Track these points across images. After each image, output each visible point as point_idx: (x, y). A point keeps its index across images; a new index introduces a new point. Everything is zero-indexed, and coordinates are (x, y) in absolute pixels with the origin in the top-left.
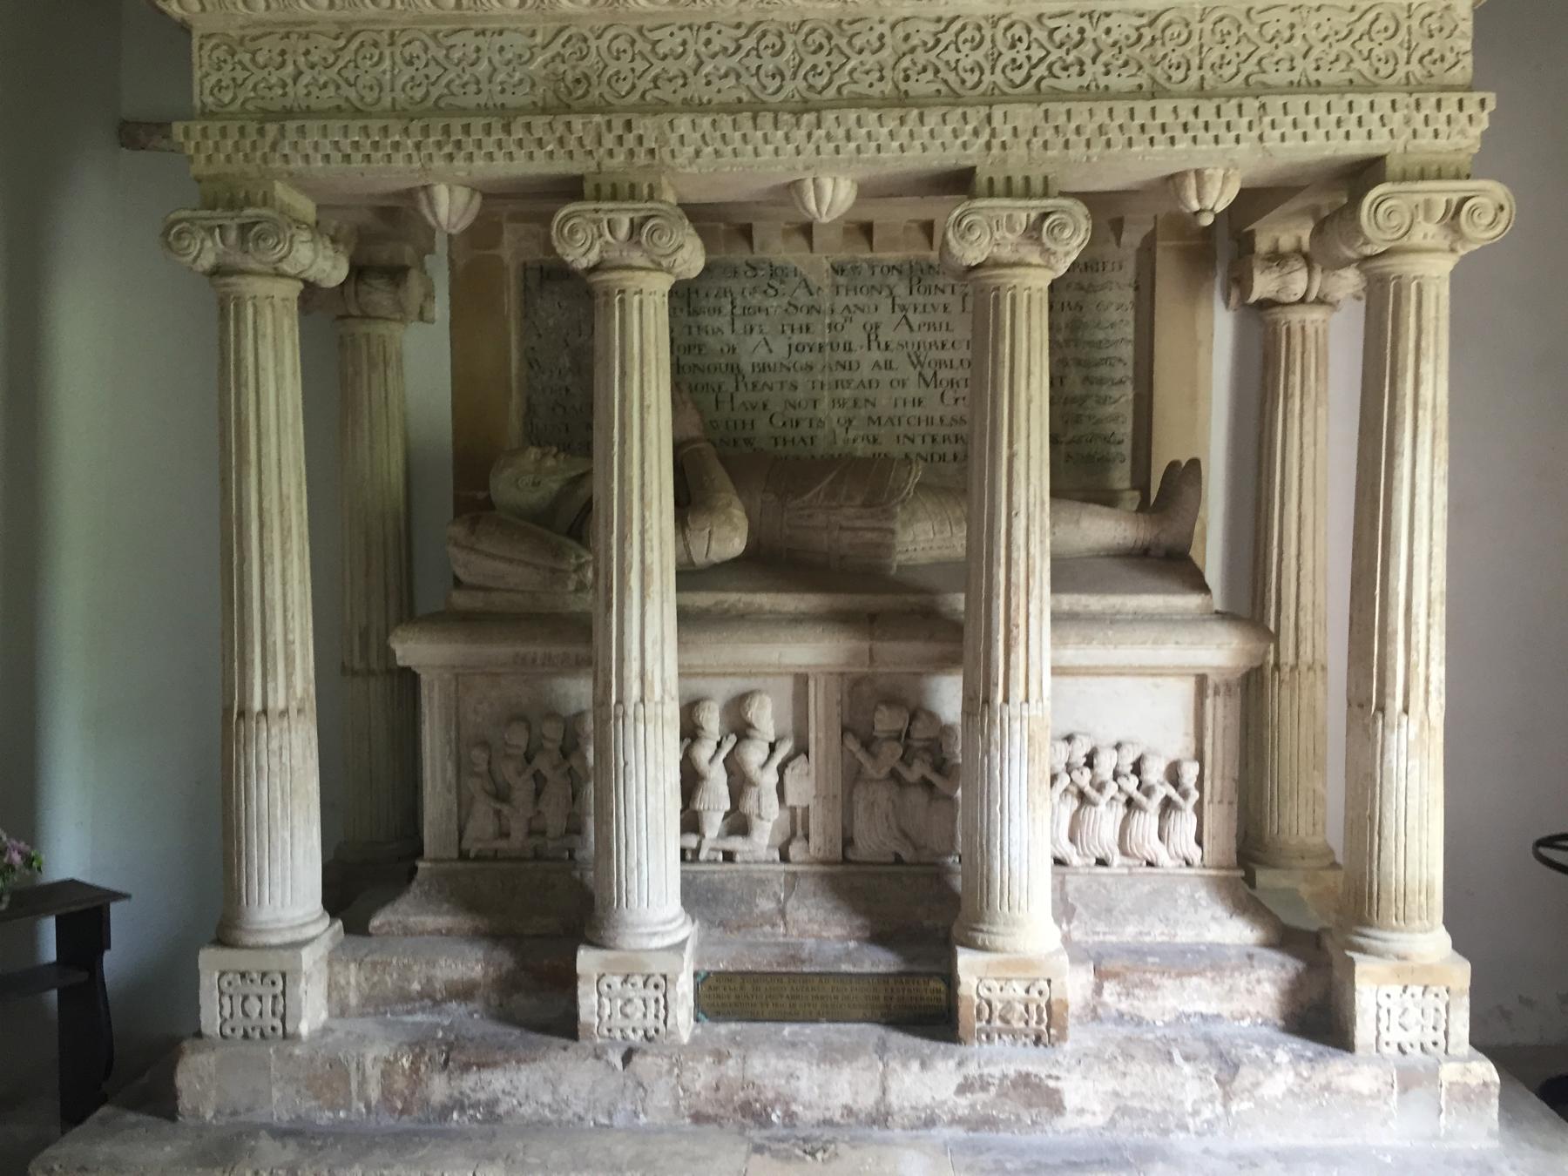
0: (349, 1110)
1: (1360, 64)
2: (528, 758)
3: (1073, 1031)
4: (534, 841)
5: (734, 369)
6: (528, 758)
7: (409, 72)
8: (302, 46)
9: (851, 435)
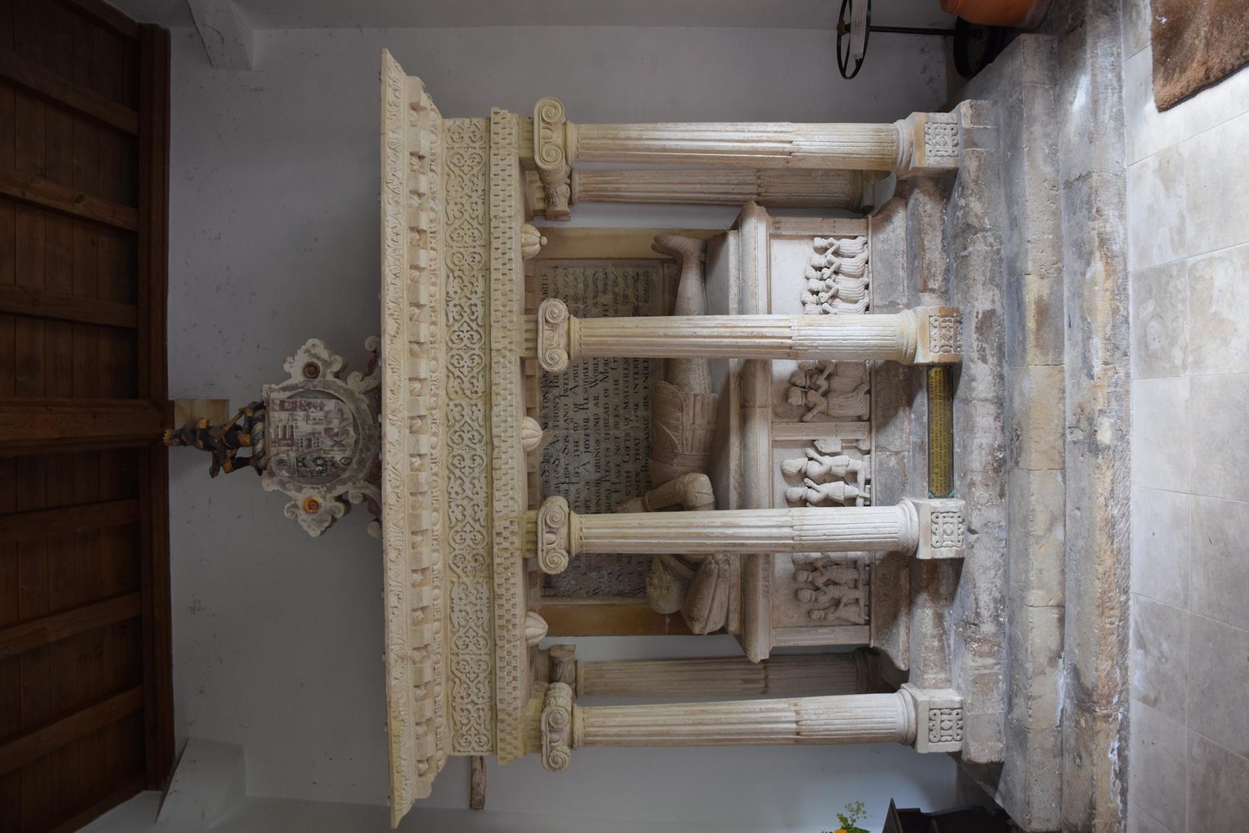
0: (997, 674)
1: (475, 171)
2: (817, 589)
3: (955, 305)
4: (860, 585)
5: (598, 482)
6: (817, 589)
7: (471, 646)
8: (458, 700)
9: (633, 418)
